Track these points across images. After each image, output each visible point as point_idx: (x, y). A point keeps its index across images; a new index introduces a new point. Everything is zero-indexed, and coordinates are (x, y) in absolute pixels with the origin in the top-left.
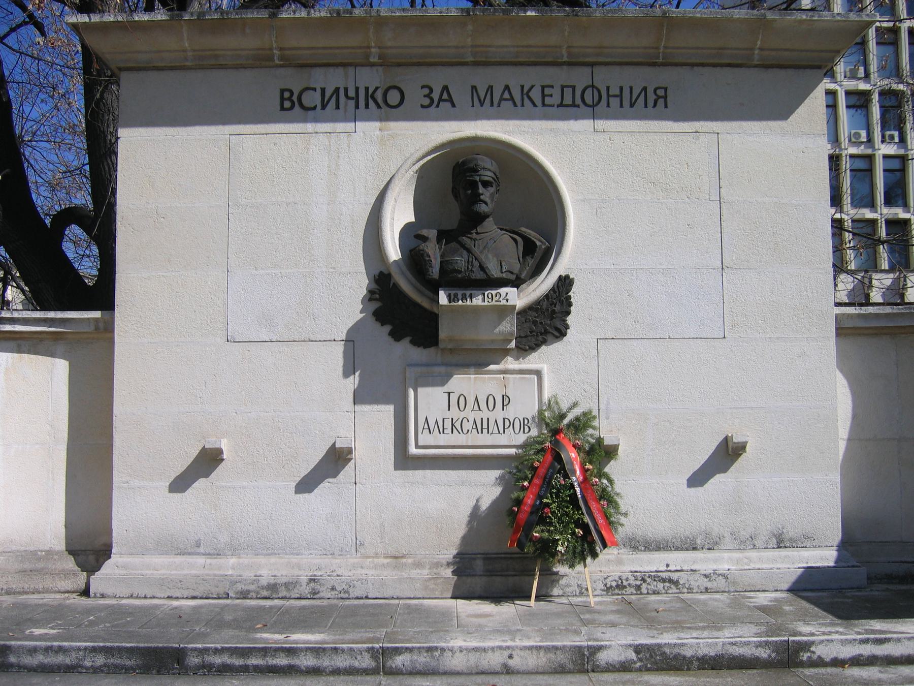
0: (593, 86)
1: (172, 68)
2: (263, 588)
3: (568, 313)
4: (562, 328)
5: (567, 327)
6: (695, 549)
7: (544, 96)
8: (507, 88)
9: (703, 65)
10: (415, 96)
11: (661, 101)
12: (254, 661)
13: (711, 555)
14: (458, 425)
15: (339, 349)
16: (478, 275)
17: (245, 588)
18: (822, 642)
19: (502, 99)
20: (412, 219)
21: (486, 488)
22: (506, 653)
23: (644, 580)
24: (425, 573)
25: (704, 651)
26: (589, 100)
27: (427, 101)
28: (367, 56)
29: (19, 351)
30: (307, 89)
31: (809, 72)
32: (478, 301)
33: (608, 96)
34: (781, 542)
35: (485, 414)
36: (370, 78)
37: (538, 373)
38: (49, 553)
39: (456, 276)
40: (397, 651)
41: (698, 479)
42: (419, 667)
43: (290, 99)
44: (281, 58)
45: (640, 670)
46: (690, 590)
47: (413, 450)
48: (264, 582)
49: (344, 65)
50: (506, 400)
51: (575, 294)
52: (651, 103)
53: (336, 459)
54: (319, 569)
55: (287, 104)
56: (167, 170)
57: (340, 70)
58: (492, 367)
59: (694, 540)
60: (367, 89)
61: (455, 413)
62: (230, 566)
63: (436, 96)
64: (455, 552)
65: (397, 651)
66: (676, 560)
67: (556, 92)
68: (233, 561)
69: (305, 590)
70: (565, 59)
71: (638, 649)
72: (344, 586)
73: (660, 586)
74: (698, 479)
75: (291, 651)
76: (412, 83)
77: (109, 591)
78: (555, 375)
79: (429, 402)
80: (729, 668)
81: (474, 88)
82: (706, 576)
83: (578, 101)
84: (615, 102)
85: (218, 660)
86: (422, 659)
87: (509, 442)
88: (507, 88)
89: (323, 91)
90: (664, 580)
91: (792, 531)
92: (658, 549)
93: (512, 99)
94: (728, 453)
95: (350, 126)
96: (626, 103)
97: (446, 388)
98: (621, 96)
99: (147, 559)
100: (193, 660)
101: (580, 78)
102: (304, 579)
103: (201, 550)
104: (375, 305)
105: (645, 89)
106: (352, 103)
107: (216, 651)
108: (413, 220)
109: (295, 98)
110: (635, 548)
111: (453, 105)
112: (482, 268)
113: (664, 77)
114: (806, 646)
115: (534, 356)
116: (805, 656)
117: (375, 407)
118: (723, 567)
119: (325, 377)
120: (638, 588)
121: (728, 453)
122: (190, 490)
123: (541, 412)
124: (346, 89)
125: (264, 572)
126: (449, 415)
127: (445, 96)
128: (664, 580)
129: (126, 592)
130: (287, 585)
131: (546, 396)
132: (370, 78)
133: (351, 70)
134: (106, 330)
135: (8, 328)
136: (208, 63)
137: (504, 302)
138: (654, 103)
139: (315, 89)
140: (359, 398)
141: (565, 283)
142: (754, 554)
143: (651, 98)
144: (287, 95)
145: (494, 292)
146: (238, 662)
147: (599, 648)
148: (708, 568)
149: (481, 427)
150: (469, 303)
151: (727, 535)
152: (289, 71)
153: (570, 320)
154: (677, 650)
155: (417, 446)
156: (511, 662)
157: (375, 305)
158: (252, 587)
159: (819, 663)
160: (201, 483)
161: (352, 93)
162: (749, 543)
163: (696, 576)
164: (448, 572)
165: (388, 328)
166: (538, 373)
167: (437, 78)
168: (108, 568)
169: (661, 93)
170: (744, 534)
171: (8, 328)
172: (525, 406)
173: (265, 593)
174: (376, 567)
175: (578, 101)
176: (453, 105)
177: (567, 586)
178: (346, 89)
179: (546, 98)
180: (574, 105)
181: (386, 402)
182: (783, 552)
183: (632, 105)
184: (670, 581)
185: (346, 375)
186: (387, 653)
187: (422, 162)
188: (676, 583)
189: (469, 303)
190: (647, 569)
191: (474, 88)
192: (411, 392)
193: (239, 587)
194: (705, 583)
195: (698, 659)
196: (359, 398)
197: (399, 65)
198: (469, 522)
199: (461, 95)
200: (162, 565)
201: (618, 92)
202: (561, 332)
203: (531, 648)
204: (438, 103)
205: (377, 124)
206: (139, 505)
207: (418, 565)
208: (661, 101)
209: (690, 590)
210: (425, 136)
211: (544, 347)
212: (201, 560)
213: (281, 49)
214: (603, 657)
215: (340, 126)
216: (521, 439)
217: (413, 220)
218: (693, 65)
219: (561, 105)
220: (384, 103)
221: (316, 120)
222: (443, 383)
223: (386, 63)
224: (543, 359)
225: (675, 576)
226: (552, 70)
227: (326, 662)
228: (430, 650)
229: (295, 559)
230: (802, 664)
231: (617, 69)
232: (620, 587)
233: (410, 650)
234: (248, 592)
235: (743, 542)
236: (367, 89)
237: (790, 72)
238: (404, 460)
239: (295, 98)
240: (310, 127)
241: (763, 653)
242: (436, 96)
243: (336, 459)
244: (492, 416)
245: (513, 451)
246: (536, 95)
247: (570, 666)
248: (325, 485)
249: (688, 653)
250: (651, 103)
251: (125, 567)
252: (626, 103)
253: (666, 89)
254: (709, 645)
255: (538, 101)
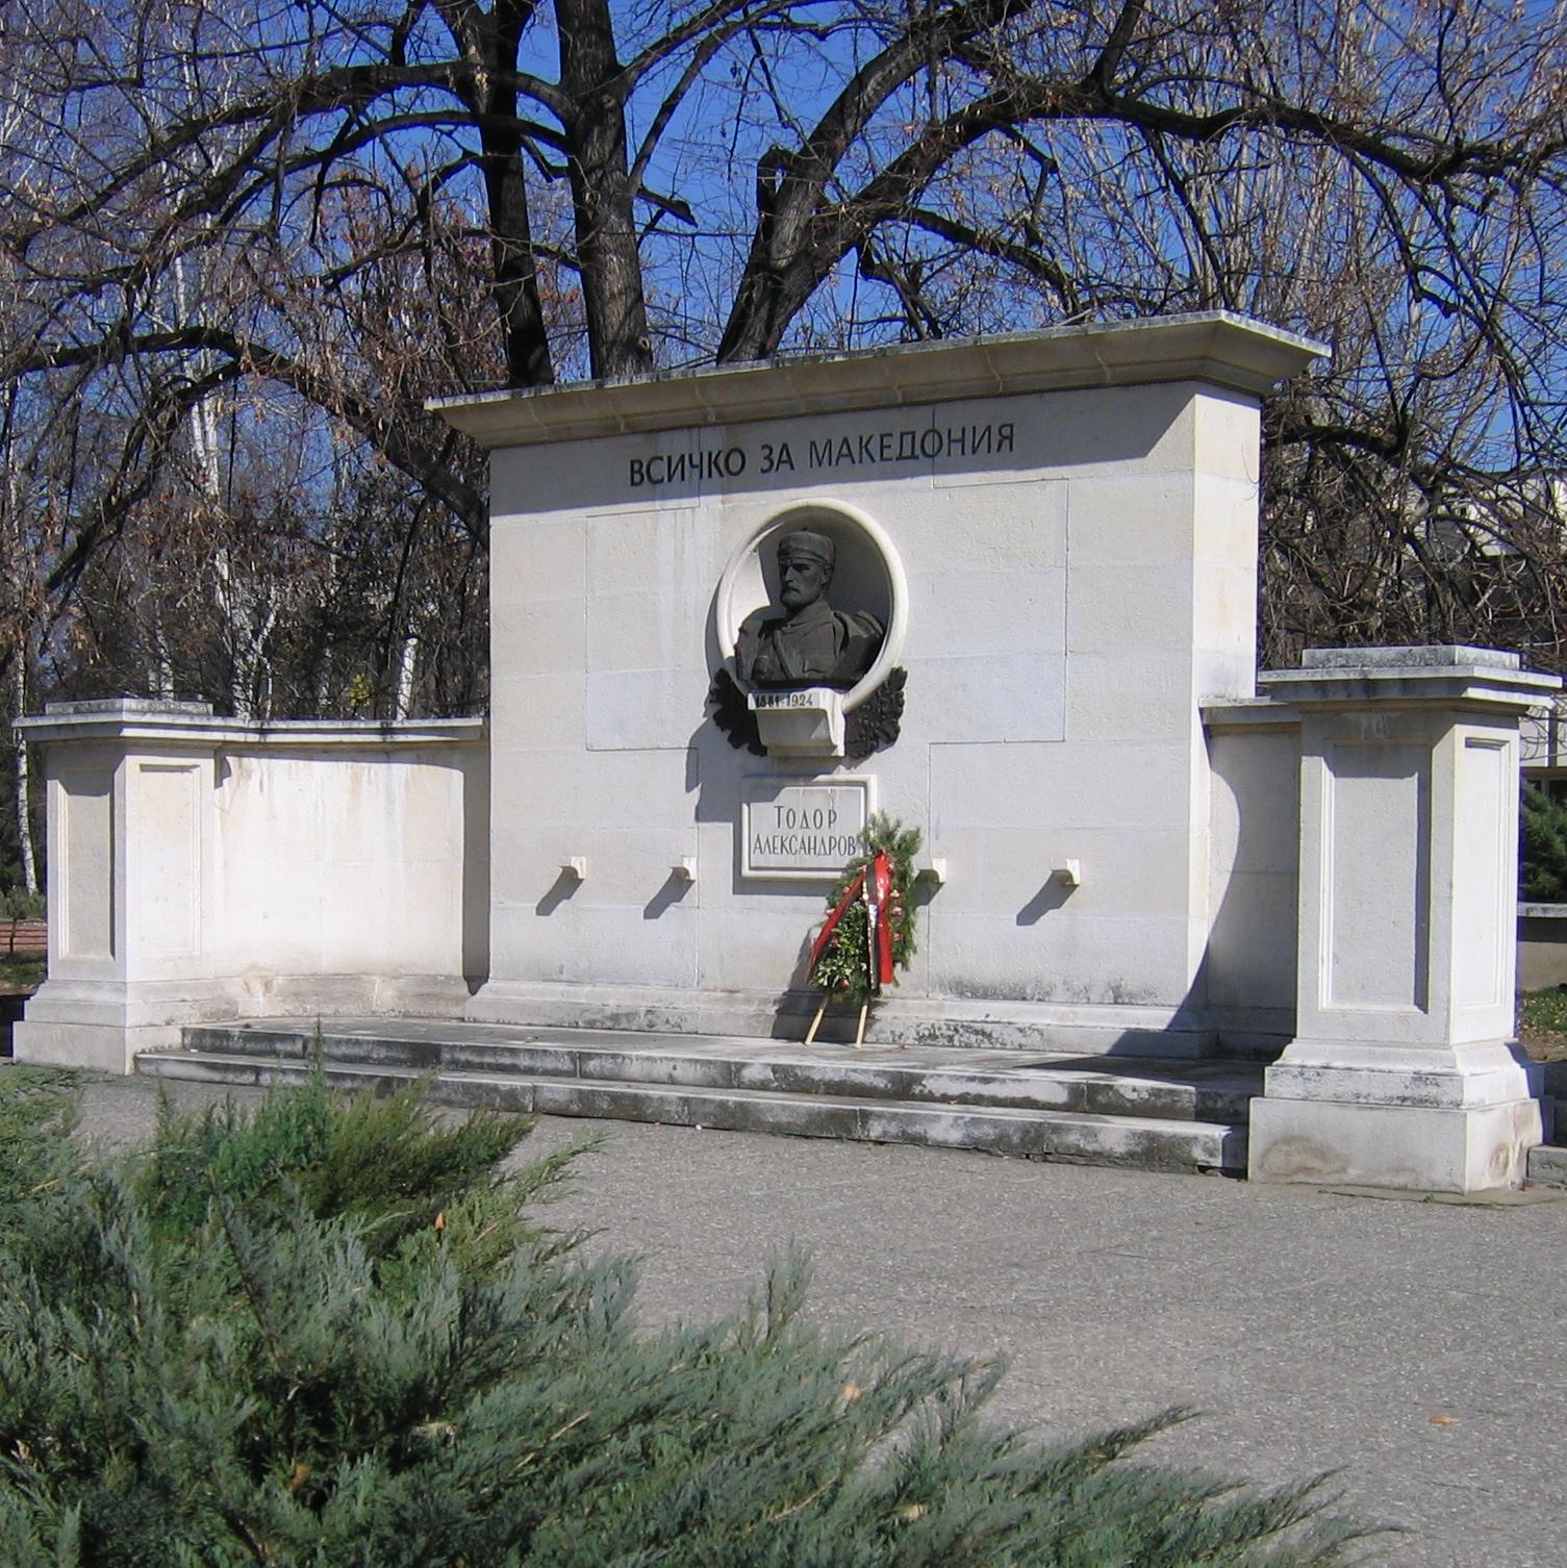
0: (934, 431)
1: (535, 444)
2: (606, 1018)
3: (898, 714)
4: (892, 733)
5: (897, 731)
6: (1024, 999)
7: (882, 448)
8: (846, 440)
9: (1053, 390)
10: (756, 459)
11: (1006, 443)
12: (488, 1059)
13: (1042, 1006)
14: (787, 844)
15: (682, 758)
16: (777, 676)
17: (593, 1017)
18: (932, 1076)
19: (840, 455)
20: (762, 600)
21: (808, 916)
22: (671, 1064)
23: (956, 1030)
24: (752, 1009)
25: (830, 1076)
26: (929, 450)
27: (767, 464)
28: (705, 417)
29: (419, 761)
30: (654, 458)
31: (1177, 385)
32: (783, 705)
33: (950, 441)
34: (1118, 997)
35: (812, 832)
36: (713, 441)
37: (864, 784)
38: (448, 977)
39: (804, 664)
40: (590, 1056)
41: (1028, 916)
42: (606, 1073)
43: (640, 472)
44: (627, 426)
45: (775, 1090)
46: (1004, 1046)
47: (746, 872)
48: (608, 1012)
49: (690, 427)
50: (833, 817)
51: (909, 692)
52: (995, 446)
53: (679, 883)
54: (660, 1001)
55: (637, 478)
56: (539, 559)
57: (686, 432)
58: (821, 778)
59: (1023, 989)
60: (710, 455)
61: (784, 831)
62: (584, 995)
63: (775, 457)
64: (786, 989)
65: (590, 1056)
66: (998, 1009)
67: (895, 442)
68: (588, 988)
69: (643, 1021)
70: (900, 400)
71: (775, 1069)
72: (676, 1019)
73: (973, 1038)
74: (1028, 916)
75: (513, 1051)
76: (753, 441)
77: (480, 1016)
78: (881, 789)
79: (759, 818)
80: (851, 1095)
81: (813, 444)
82: (1021, 1030)
83: (918, 451)
84: (956, 448)
85: (463, 1057)
86: (609, 1065)
87: (834, 863)
88: (846, 440)
89: (669, 459)
90: (976, 1032)
91: (1130, 985)
92: (985, 997)
93: (850, 454)
94: (1060, 887)
95: (694, 501)
96: (968, 449)
97: (776, 802)
98: (962, 440)
99: (516, 985)
100: (446, 1056)
101: (919, 420)
102: (643, 1010)
103: (564, 977)
104: (717, 707)
105: (989, 428)
106: (697, 471)
107: (462, 1048)
108: (768, 603)
109: (644, 470)
110: (961, 994)
111: (792, 467)
112: (783, 668)
113: (1008, 411)
114: (917, 1079)
115: (866, 764)
116: (917, 1089)
117: (717, 824)
118: (1042, 1022)
119: (668, 787)
120: (951, 1039)
121: (1060, 887)
122: (554, 913)
123: (866, 830)
124: (691, 457)
125: (612, 1002)
126: (779, 832)
127: (785, 457)
128: (976, 1032)
129: (493, 1017)
130: (627, 1015)
131: (874, 809)
132: (713, 441)
133: (695, 431)
134: (484, 734)
135: (401, 738)
136: (561, 437)
137: (807, 706)
138: (998, 447)
139: (661, 459)
140: (701, 815)
141: (897, 678)
142: (1082, 1009)
143: (995, 438)
144: (636, 467)
145: (798, 694)
146: (476, 1059)
147: (744, 1065)
148: (1023, 1021)
149: (807, 847)
150: (775, 707)
151: (1059, 984)
152: (638, 439)
153: (901, 722)
154: (806, 1073)
155: (751, 868)
156: (675, 1073)
157: (717, 707)
158: (598, 1017)
159: (929, 1098)
160: (563, 905)
161: (696, 461)
162: (1082, 996)
163: (1010, 1029)
164: (772, 1010)
165: (728, 733)
166: (864, 784)
167: (776, 434)
168: (484, 991)
169: (1006, 431)
170: (1078, 984)
171: (401, 738)
172: (852, 824)
173: (609, 1024)
174: (709, 1001)
175: (918, 451)
176: (792, 467)
177: (882, 1031)
178: (691, 457)
179: (885, 451)
180: (913, 456)
181: (727, 820)
182: (1119, 1009)
183: (974, 452)
184: (983, 1033)
185: (689, 789)
186: (584, 1057)
187: (758, 540)
188: (989, 1036)
189: (775, 707)
190: (964, 1018)
191: (813, 444)
192: (745, 807)
193: (588, 1016)
194: (1018, 1038)
195: (826, 1084)
196: (701, 815)
197: (741, 422)
198: (800, 956)
199: (800, 455)
200: (529, 992)
201: (960, 436)
202: (891, 737)
203: (690, 1060)
204: (779, 467)
205: (720, 497)
206: (515, 928)
207: (747, 1001)
208: (1006, 443)
209: (1004, 1046)
210: (766, 505)
211: (875, 754)
212: (561, 987)
213: (624, 416)
214: (748, 1074)
215: (685, 502)
216: (845, 861)
217: (768, 603)
218: (1042, 392)
219: (900, 458)
220: (724, 472)
221: (664, 497)
222: (772, 800)
223: (723, 421)
224: (875, 770)
225: (988, 1028)
226: (893, 414)
227: (538, 1063)
228: (614, 1056)
229: (641, 990)
230: (913, 1097)
231: (960, 404)
232: (933, 1036)
233: (599, 1055)
234: (595, 1021)
235: (1076, 994)
236: (710, 455)
237: (1155, 388)
238: (743, 885)
239: (644, 470)
240: (657, 504)
241: (881, 1083)
242: (775, 457)
243: (679, 883)
244: (819, 834)
245: (838, 875)
246: (874, 447)
247: (720, 1081)
248: (671, 909)
249: (817, 1077)
250: (995, 446)
251: (497, 992)
252: (968, 449)
253: (1011, 426)
254: (834, 1070)
255: (877, 458)
